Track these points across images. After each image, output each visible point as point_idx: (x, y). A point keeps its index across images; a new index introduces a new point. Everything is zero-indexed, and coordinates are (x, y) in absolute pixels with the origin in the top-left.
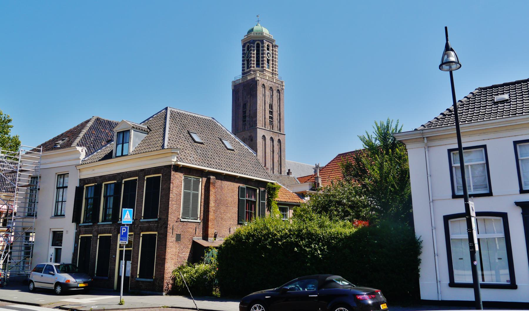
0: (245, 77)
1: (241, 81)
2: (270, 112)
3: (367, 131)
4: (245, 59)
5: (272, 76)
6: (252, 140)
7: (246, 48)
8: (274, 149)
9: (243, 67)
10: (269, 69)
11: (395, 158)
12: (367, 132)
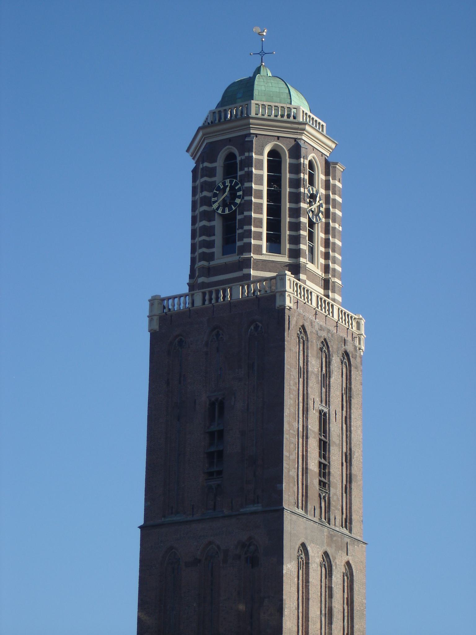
0: (213, 289)
3: (290, 316)
4: (214, 211)
5: (322, 291)
6: (253, 561)
7: (219, 164)
8: (333, 604)
11: (243, 184)
12: (289, 316)
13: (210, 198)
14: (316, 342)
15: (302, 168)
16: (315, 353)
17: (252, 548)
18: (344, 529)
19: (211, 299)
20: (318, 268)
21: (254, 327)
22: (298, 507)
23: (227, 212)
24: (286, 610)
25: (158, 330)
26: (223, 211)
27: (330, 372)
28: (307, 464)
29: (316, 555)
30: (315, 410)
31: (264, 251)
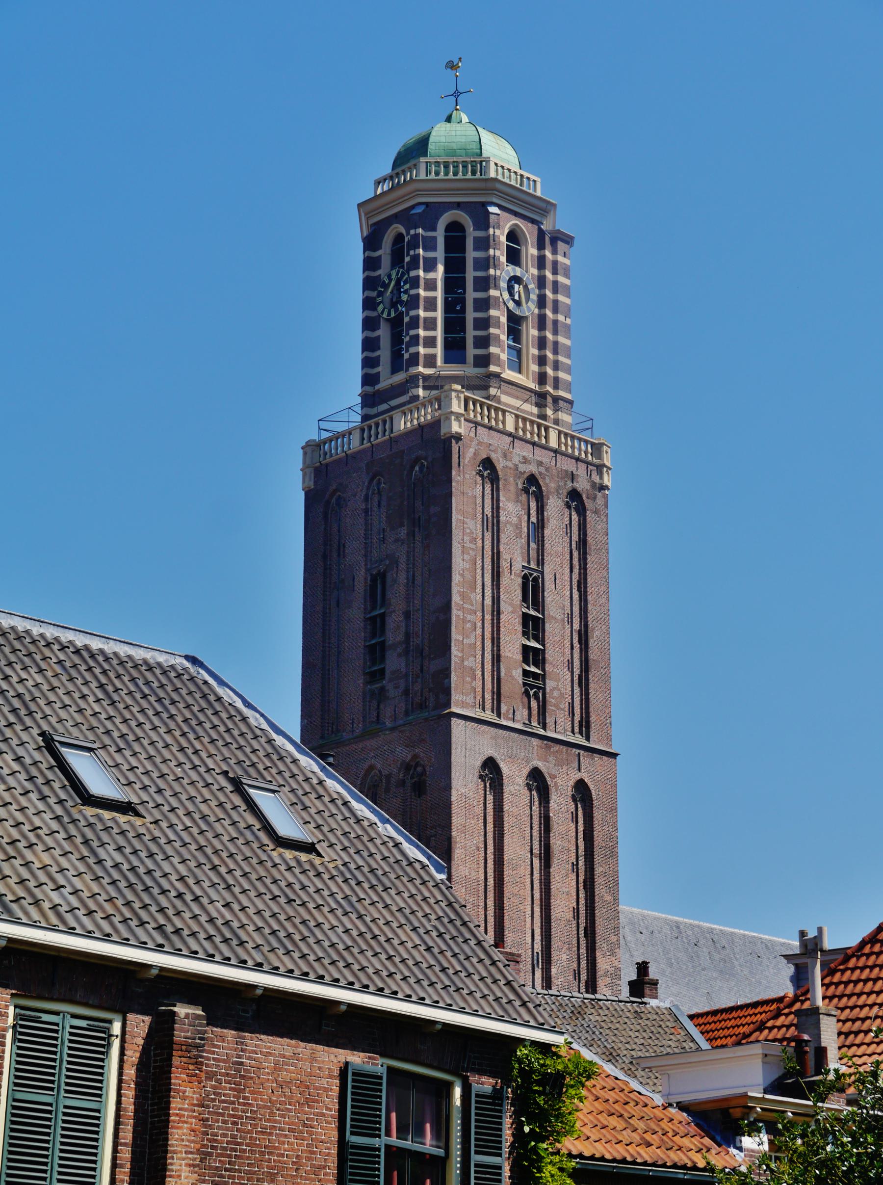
1: (355, 443)
2: (525, 624)
4: (379, 316)
6: (419, 788)
7: (385, 252)
9: (368, 363)
10: (520, 372)
13: (374, 299)
14: (515, 481)
15: (491, 241)
16: (512, 496)
17: (419, 769)
18: (578, 735)
19: (370, 436)
20: (528, 378)
21: (419, 468)
22: (483, 709)
23: (393, 315)
24: (456, 851)
25: (313, 487)
26: (389, 314)
27: (543, 520)
28: (499, 650)
29: (517, 773)
30: (513, 573)
31: (439, 362)
